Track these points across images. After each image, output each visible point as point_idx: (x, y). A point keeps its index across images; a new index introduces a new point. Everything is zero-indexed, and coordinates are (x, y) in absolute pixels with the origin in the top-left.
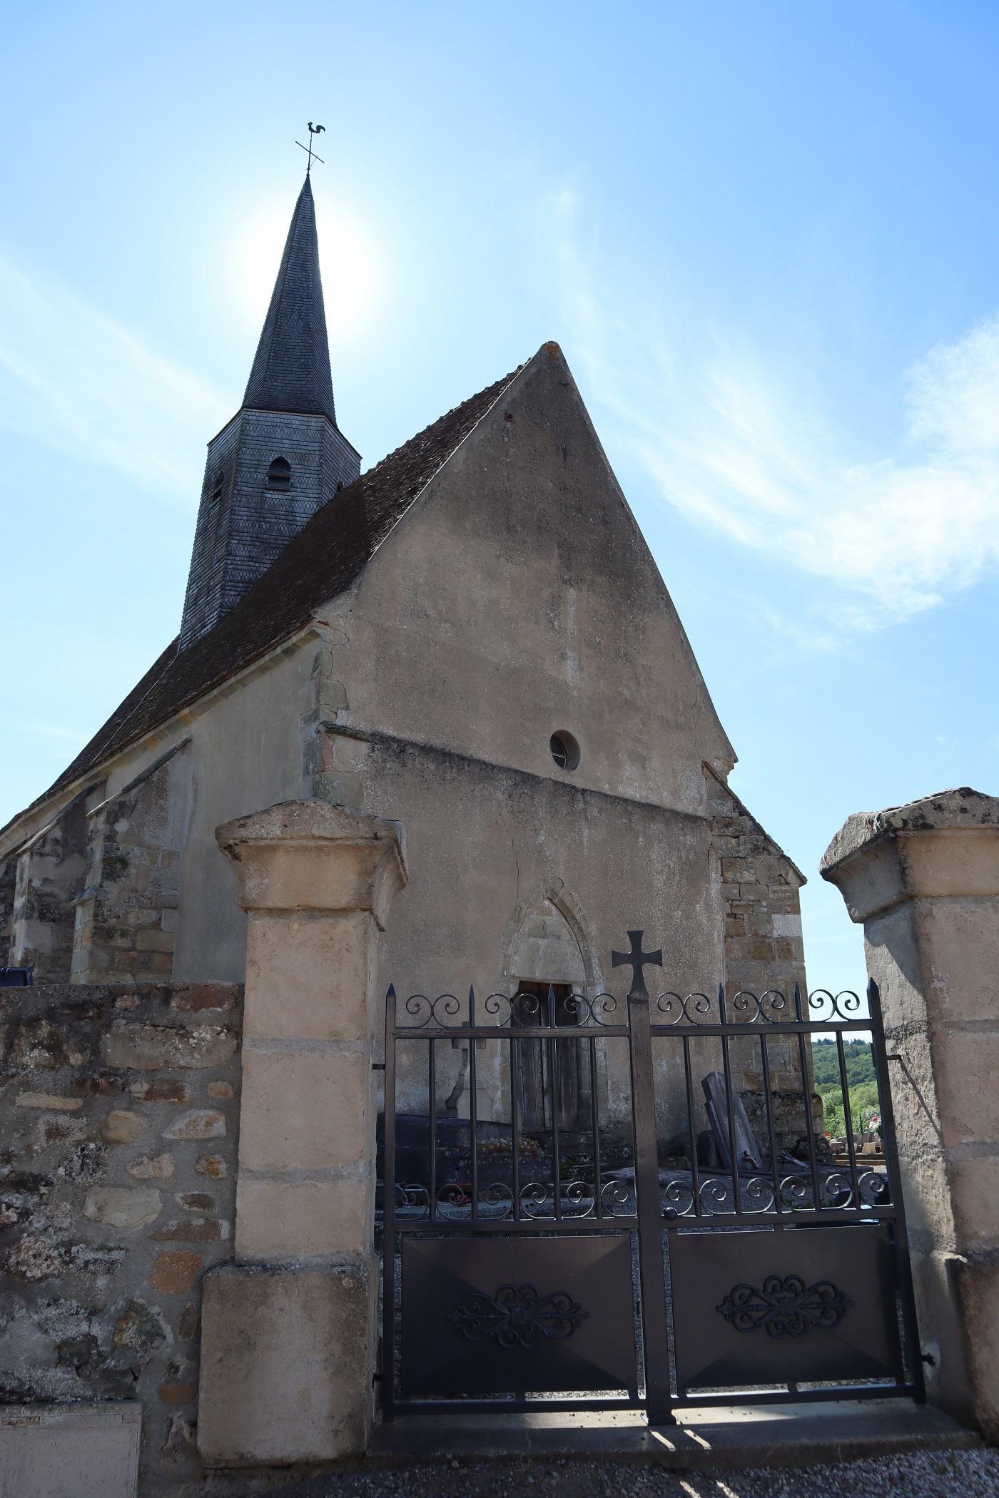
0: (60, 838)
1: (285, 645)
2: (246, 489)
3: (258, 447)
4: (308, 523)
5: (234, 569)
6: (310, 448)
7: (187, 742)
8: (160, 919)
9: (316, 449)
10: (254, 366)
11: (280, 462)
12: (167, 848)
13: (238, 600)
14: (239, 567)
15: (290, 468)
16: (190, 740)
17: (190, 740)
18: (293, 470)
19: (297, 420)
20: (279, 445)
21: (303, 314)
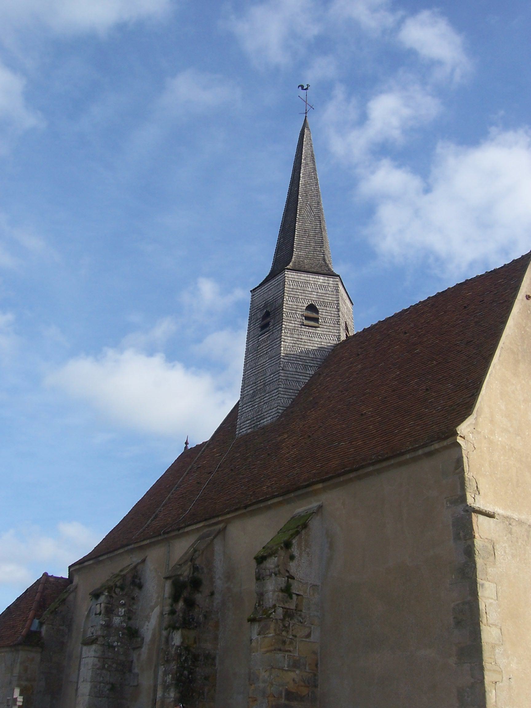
0: (171, 580)
1: (427, 450)
2: (290, 325)
3: (296, 296)
4: (333, 350)
5: (286, 380)
6: (330, 299)
7: (320, 507)
8: (311, 631)
9: (335, 299)
10: (279, 239)
11: (312, 308)
12: (312, 583)
13: (290, 402)
14: (290, 379)
15: (318, 311)
16: (322, 506)
17: (322, 506)
18: (320, 313)
19: (321, 279)
20: (310, 295)
21: (313, 207)
